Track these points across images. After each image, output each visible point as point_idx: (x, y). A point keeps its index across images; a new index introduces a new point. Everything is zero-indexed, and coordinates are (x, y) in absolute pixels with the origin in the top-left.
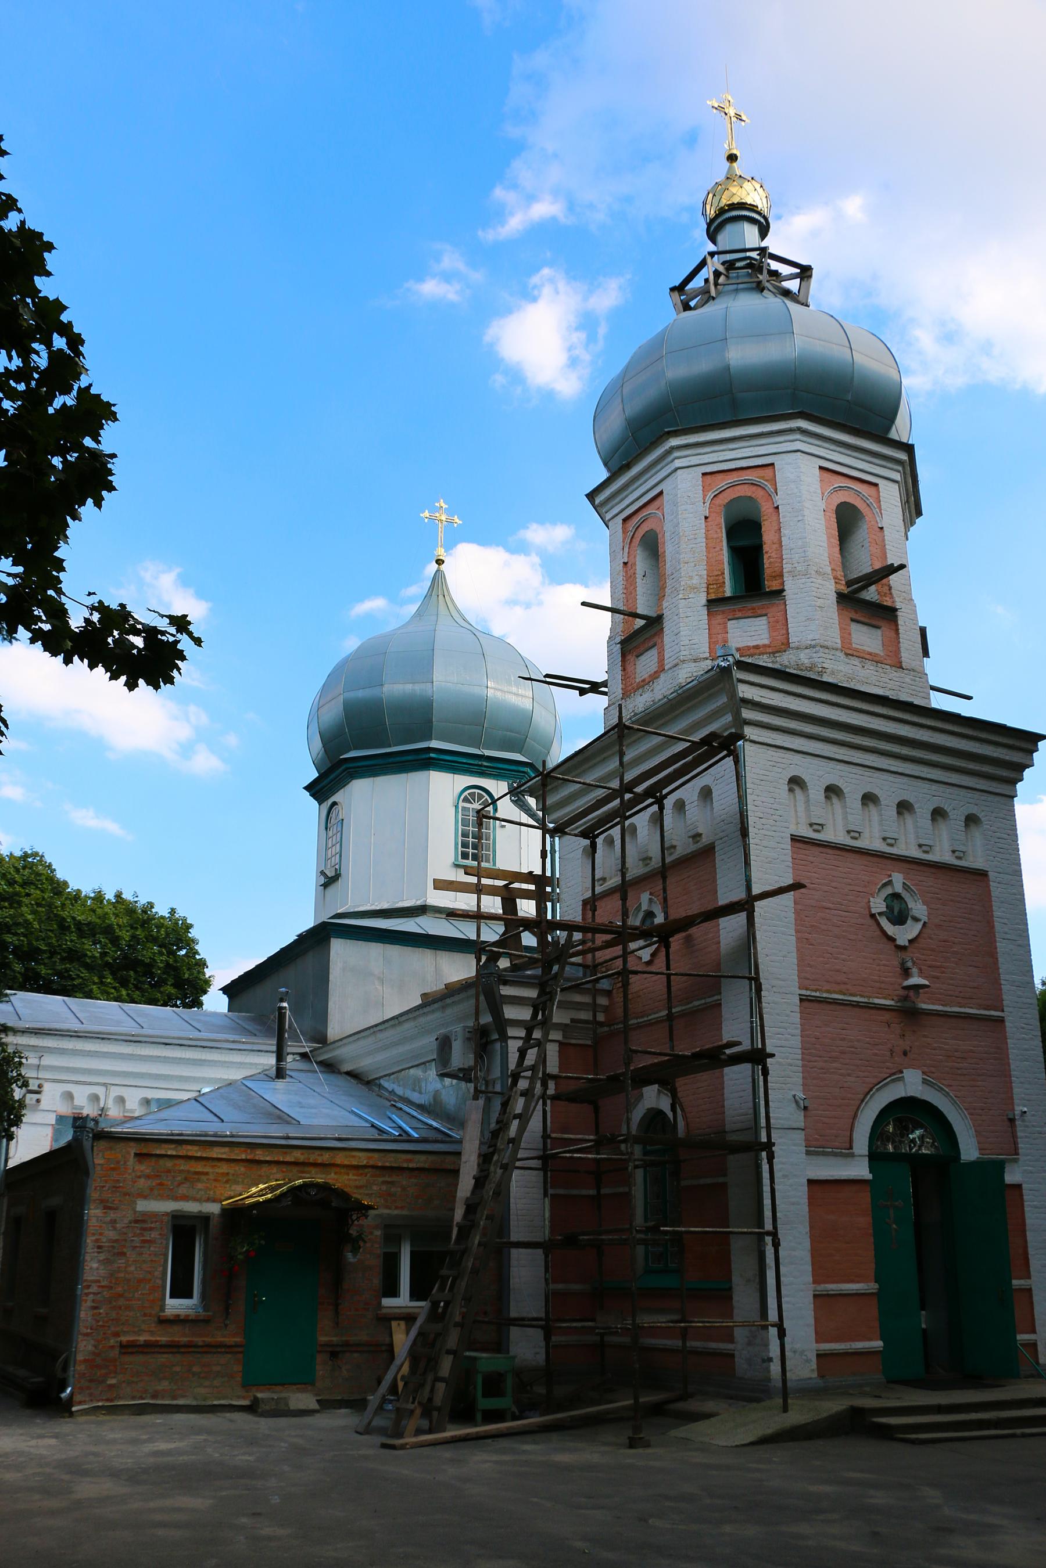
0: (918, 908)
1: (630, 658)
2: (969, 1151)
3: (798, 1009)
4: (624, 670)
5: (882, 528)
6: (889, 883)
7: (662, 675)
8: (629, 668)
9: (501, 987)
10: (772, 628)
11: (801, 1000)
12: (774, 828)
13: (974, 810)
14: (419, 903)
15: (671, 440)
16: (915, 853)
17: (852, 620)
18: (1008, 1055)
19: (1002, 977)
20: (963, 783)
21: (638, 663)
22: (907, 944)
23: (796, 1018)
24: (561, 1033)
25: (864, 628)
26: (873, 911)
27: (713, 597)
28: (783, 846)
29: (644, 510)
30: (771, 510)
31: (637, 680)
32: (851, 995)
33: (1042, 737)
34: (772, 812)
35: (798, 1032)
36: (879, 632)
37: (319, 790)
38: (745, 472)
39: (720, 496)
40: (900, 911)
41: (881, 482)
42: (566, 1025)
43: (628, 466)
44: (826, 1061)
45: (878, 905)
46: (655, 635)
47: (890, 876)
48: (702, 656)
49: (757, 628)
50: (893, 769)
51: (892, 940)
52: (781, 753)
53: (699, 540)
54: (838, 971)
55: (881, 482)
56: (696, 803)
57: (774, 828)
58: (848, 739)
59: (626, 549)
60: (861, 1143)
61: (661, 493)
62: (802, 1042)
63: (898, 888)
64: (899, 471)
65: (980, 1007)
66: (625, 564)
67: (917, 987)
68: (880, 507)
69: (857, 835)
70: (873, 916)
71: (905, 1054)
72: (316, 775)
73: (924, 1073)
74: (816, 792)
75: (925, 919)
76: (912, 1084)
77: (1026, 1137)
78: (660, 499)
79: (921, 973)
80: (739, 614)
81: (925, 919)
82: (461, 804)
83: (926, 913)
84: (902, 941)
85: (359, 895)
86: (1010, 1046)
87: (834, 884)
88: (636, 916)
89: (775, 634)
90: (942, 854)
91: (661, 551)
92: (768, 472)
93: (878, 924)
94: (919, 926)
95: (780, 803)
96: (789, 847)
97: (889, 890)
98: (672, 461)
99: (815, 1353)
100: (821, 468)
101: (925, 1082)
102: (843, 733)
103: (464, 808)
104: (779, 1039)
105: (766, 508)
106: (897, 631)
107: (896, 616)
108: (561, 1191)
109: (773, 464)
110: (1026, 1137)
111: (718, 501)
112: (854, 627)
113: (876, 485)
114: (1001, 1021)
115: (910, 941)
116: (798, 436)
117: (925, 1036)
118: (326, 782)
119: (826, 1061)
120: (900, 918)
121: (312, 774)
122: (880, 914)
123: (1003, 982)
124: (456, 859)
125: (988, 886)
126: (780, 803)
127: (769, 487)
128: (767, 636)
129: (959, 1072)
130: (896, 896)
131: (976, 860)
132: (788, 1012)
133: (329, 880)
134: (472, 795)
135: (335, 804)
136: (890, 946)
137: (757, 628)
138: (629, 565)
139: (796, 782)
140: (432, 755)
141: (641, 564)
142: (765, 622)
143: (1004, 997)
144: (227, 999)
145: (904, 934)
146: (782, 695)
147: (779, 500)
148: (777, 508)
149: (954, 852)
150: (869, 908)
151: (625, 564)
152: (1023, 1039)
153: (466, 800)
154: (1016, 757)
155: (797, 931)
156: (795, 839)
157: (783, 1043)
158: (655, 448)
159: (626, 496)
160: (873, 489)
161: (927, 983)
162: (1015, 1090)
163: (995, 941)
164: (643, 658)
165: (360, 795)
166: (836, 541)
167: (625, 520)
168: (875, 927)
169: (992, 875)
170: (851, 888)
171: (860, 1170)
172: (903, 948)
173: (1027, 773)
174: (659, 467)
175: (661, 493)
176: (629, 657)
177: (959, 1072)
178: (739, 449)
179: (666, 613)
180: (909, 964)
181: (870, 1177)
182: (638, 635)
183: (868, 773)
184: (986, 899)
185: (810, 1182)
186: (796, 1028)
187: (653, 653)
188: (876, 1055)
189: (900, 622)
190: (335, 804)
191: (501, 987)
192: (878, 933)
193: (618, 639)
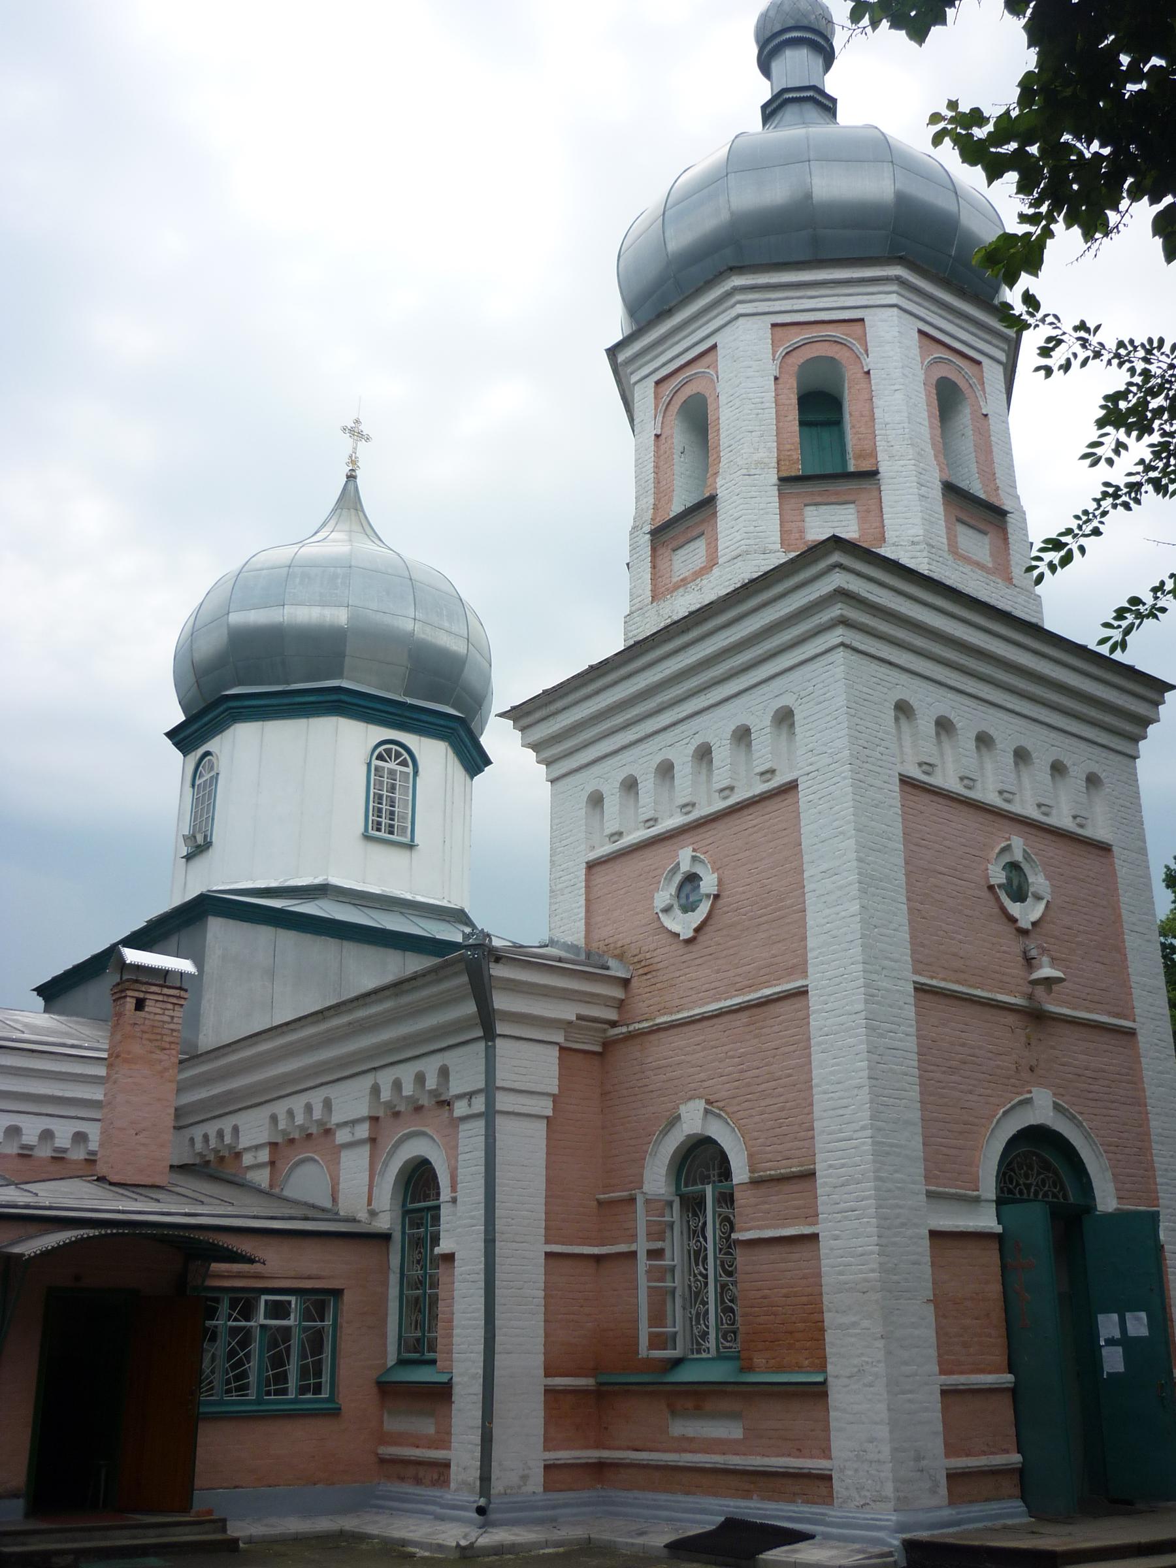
0: (1038, 881)
1: (664, 552)
2: (1107, 1200)
3: (912, 1000)
4: (654, 567)
5: (986, 415)
6: (1007, 849)
7: (716, 570)
8: (662, 565)
9: (492, 965)
10: (862, 519)
11: (916, 989)
12: (880, 763)
13: (1095, 768)
14: (317, 881)
15: (733, 278)
16: (1034, 814)
17: (959, 520)
18: (1142, 1078)
19: (1133, 978)
20: (1084, 734)
21: (675, 558)
22: (1030, 927)
23: (910, 1012)
24: (562, 1033)
25: (970, 532)
26: (993, 881)
27: (785, 474)
28: (891, 787)
29: (687, 369)
30: (860, 375)
31: (675, 580)
32: (971, 986)
33: (1171, 687)
34: (877, 741)
35: (913, 1030)
36: (986, 540)
37: (184, 737)
38: (825, 326)
39: (794, 353)
40: (1020, 887)
41: (986, 361)
42: (570, 1023)
43: (669, 312)
44: (944, 1072)
45: (998, 876)
46: (703, 521)
47: (1009, 839)
48: (771, 547)
49: (842, 518)
50: (1009, 706)
51: (1013, 920)
52: (884, 670)
53: (768, 405)
54: (954, 955)
55: (986, 361)
56: (768, 730)
57: (880, 763)
58: (962, 662)
59: (660, 419)
60: (988, 1188)
61: (714, 347)
62: (919, 1045)
63: (1018, 856)
64: (1003, 350)
65: (1109, 1014)
66: (657, 436)
67: (1048, 982)
68: (984, 390)
69: (971, 783)
70: (991, 888)
71: (1032, 1070)
72: (182, 718)
73: (1054, 1094)
74: (926, 724)
75: (1048, 897)
76: (1041, 1110)
77: (1167, 1184)
78: (712, 354)
79: (1054, 961)
80: (819, 499)
81: (1048, 897)
82: (375, 762)
83: (1049, 890)
84: (1024, 924)
85: (224, 873)
86: (1144, 1066)
87: (947, 843)
88: (670, 880)
89: (866, 526)
90: (1062, 819)
91: (711, 417)
92: (857, 327)
93: (998, 899)
94: (1040, 908)
95: (885, 732)
96: (897, 789)
97: (1007, 859)
98: (733, 306)
99: (542, 1464)
100: (920, 332)
101: (1057, 1107)
102: (956, 653)
103: (377, 769)
104: (891, 1038)
105: (851, 373)
106: (1006, 540)
107: (1005, 522)
108: (933, 1188)
109: (862, 320)
110: (1167, 1184)
111: (791, 360)
112: (961, 529)
113: (979, 363)
114: (1131, 1033)
115: (1034, 924)
116: (895, 288)
117: (1053, 1048)
118: (195, 727)
119: (944, 1072)
120: (1019, 896)
121: (178, 717)
122: (1000, 886)
123: (1133, 985)
124: (366, 829)
125: (1112, 864)
126: (885, 732)
127: (858, 347)
128: (856, 528)
129: (1091, 1095)
130: (1014, 867)
131: (1100, 830)
132: (901, 1003)
133: (198, 847)
134: (388, 751)
135: (207, 754)
136: (1009, 929)
137: (842, 518)
138: (663, 437)
139: (903, 709)
140: (344, 698)
141: (678, 437)
142: (852, 511)
143: (1136, 1004)
144: (43, 1003)
145: (1028, 913)
146: (891, 594)
147: (870, 362)
148: (868, 373)
149: (1075, 817)
150: (987, 878)
151: (657, 436)
152: (1157, 1058)
153: (380, 757)
154: (1140, 708)
155: (908, 899)
156: (906, 782)
157: (897, 1044)
158: (711, 288)
159: (665, 351)
160: (975, 367)
161: (1061, 975)
162: (1153, 1124)
163: (1123, 933)
164: (681, 552)
165: (242, 746)
166: (937, 423)
167: (658, 383)
168: (993, 903)
169: (1114, 849)
170: (968, 850)
171: (986, 1220)
172: (1023, 932)
173: (1152, 729)
174: (715, 312)
175: (714, 347)
176: (660, 552)
177: (1091, 1095)
178: (823, 298)
179: (722, 493)
180: (1034, 953)
181: (999, 1229)
182: (677, 526)
183: (982, 707)
184: (1111, 876)
185: (934, 1234)
186: (912, 1026)
187: (700, 546)
188: (998, 1067)
189: (1010, 530)
190: (207, 754)
191: (492, 965)
192: (997, 910)
193: (647, 528)
